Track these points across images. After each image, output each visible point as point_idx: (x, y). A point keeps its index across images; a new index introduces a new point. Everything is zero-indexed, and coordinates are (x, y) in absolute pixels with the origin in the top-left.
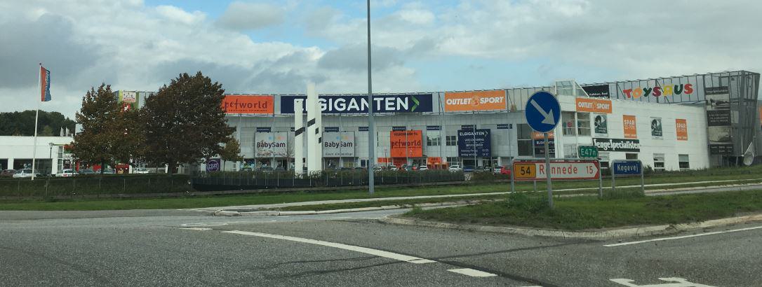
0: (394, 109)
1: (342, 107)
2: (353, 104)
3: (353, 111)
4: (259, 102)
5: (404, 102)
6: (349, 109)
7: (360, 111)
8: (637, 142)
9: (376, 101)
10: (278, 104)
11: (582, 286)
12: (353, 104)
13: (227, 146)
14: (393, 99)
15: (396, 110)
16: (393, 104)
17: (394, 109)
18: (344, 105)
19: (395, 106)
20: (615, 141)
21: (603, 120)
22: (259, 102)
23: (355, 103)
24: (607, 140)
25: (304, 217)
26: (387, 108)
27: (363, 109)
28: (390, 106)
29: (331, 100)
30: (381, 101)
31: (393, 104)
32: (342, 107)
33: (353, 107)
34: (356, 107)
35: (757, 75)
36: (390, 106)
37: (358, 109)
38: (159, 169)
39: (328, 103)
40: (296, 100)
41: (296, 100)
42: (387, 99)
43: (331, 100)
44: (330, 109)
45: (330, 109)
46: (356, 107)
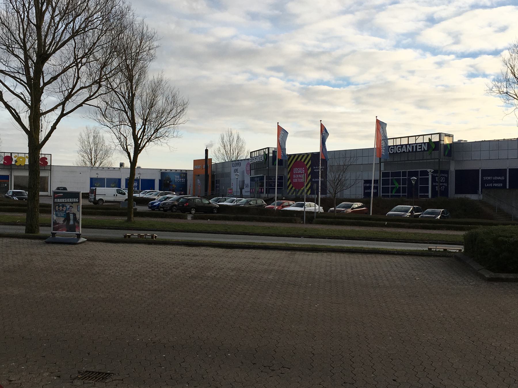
0: (420, 150)
2: (404, 149)
3: (404, 151)
9: (413, 146)
11: (517, 307)
12: (404, 149)
13: (302, 162)
14: (421, 144)
15: (421, 151)
16: (420, 147)
17: (420, 150)
19: (421, 148)
25: (300, 256)
31: (420, 147)
33: (404, 150)
34: (405, 150)
35: (194, 160)
38: (238, 199)
40: (12, 154)
41: (12, 154)
42: (418, 145)
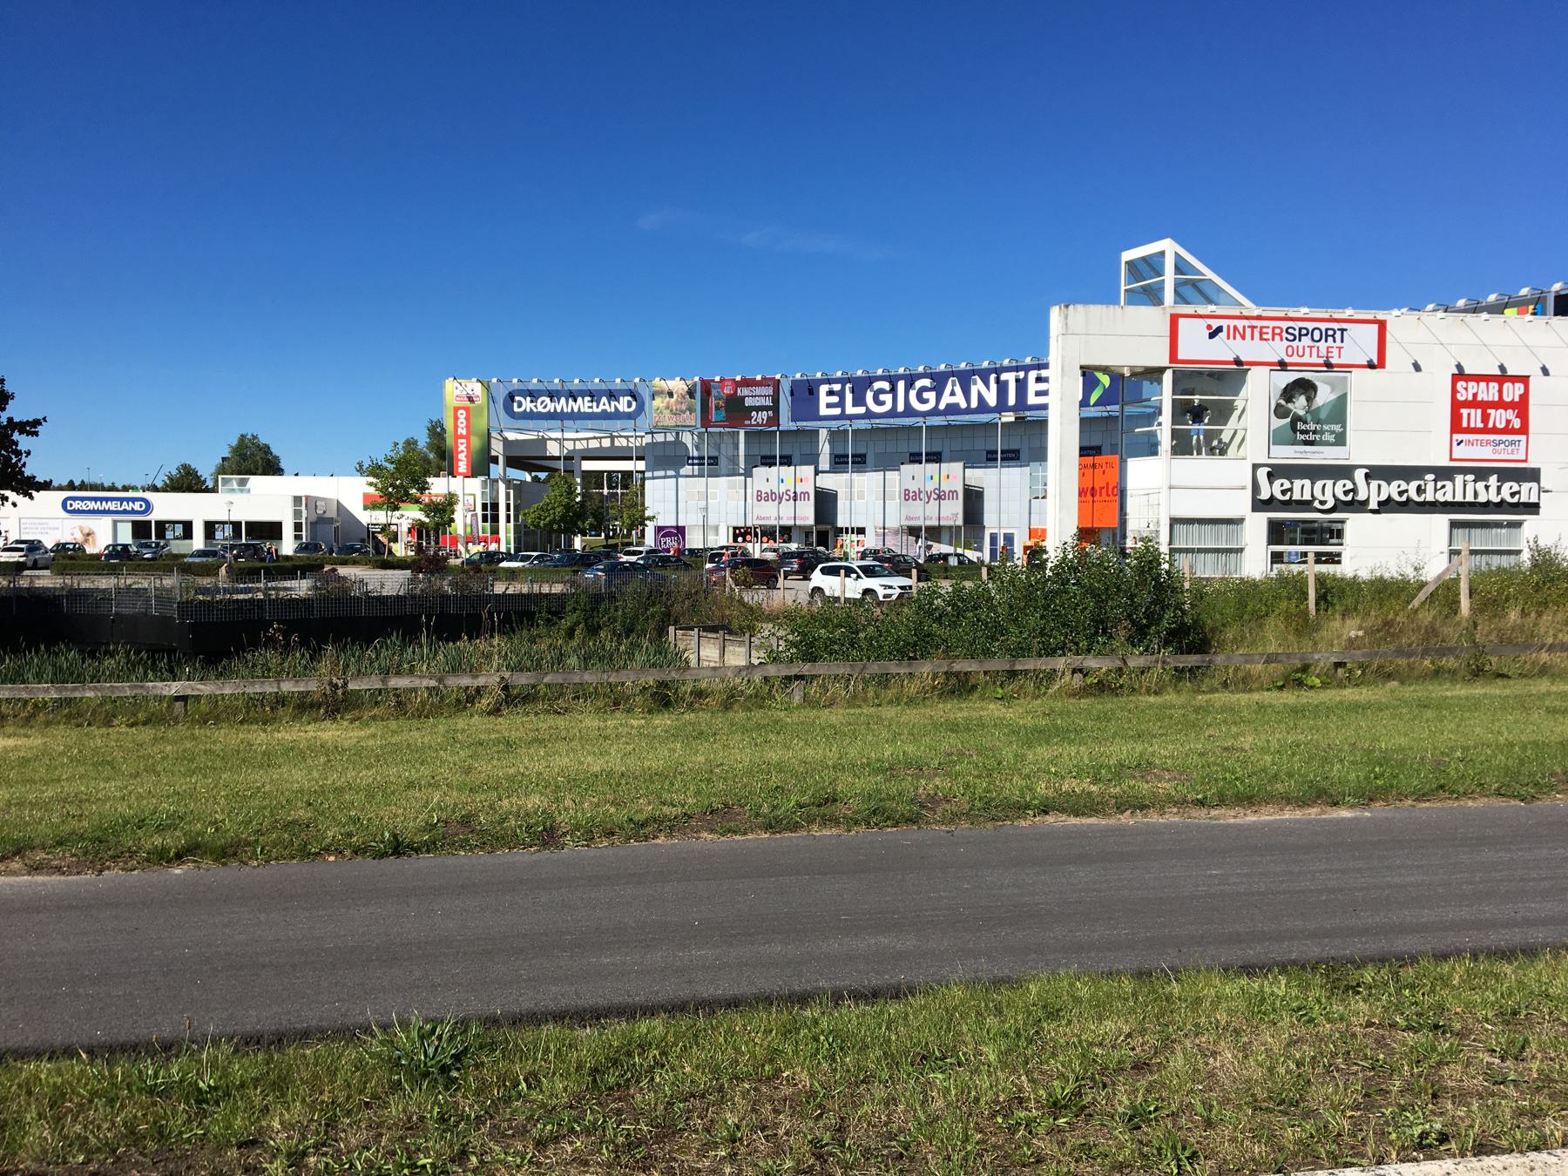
0: (837, 411)
1: (882, 403)
3: (953, 409)
4: (1107, 484)
5: (988, 388)
6: (942, 406)
7: (968, 411)
8: (1533, 475)
10: (869, 459)
12: (953, 394)
17: (837, 411)
18: (931, 396)
20: (1374, 473)
21: (1324, 396)
22: (1107, 484)
23: (958, 389)
24: (1345, 472)
26: (824, 411)
27: (974, 404)
28: (829, 406)
29: (901, 385)
30: (1017, 380)
31: (835, 399)
32: (882, 403)
33: (952, 400)
34: (959, 399)
36: (829, 406)
37: (963, 405)
39: (893, 390)
43: (901, 385)
44: (901, 408)
45: (901, 408)
46: (959, 399)
